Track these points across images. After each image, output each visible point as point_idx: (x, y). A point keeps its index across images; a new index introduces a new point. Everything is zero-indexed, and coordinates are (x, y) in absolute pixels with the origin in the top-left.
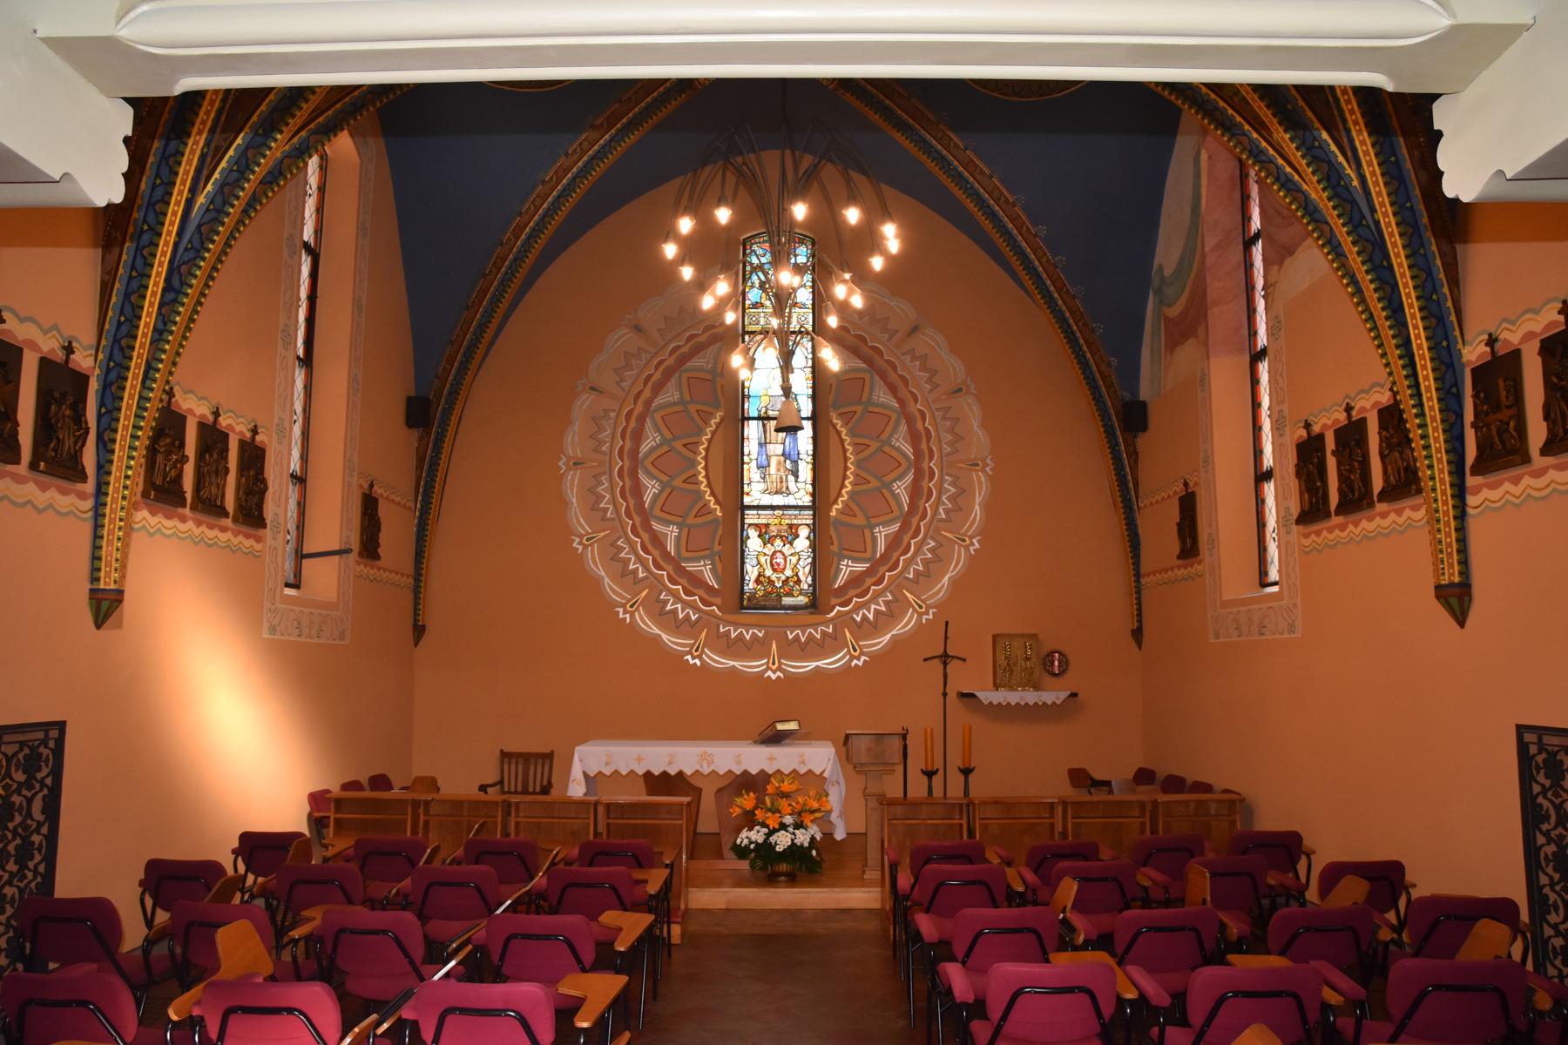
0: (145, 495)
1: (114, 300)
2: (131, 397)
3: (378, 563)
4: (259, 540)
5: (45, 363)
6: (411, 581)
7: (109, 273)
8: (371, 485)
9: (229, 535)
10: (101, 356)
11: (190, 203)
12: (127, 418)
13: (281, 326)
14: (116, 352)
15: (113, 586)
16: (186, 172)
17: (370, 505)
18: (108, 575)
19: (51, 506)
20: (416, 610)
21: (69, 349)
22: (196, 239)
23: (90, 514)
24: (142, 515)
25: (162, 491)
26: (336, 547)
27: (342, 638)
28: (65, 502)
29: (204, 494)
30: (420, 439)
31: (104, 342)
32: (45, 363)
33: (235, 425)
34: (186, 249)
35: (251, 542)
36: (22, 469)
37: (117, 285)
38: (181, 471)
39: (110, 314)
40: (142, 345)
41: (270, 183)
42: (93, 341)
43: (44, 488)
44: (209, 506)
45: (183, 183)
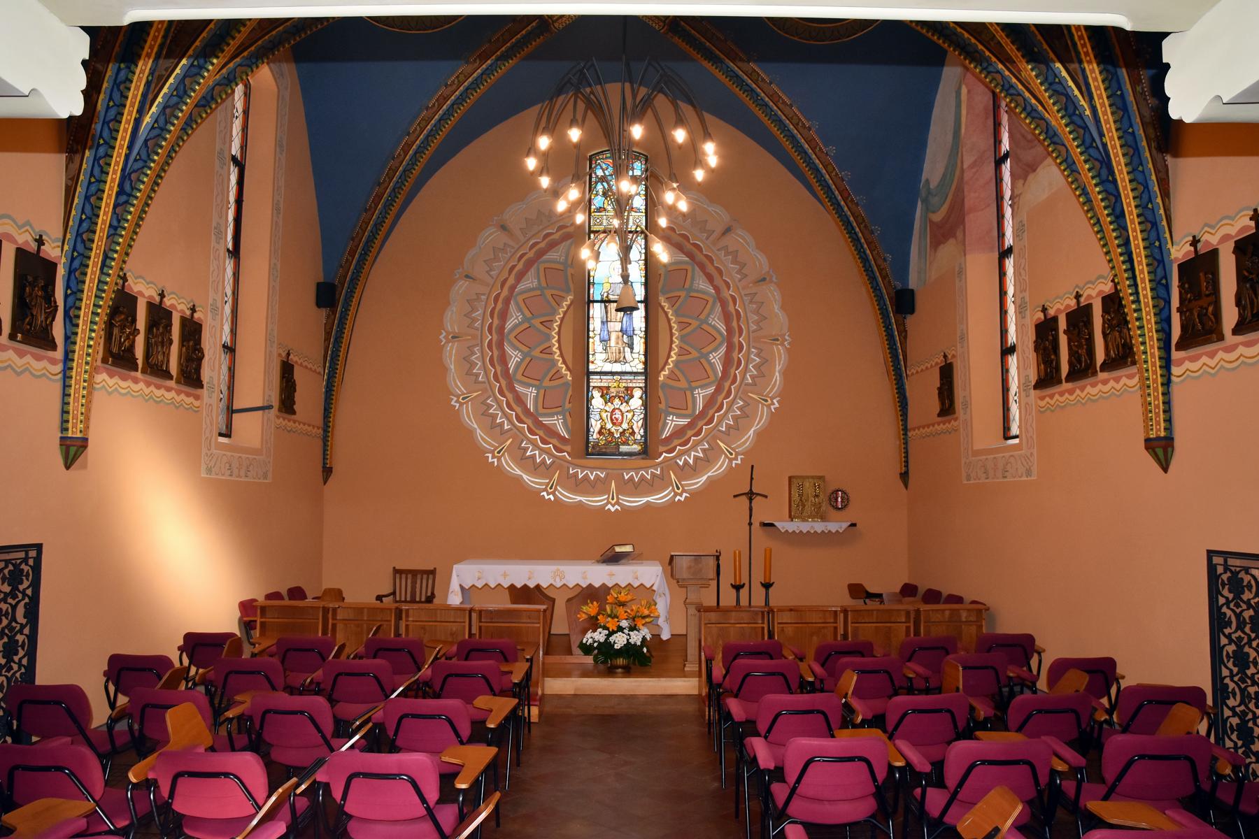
0: (104, 361)
1: (76, 201)
4: (197, 398)
6: (321, 431)
7: (72, 179)
9: (173, 394)
10: (66, 247)
11: (138, 122)
17: (287, 370)
18: (75, 426)
20: (325, 454)
21: (40, 242)
25: (120, 358)
26: (260, 404)
30: (328, 317)
31: (68, 236)
33: (178, 305)
34: (136, 160)
37: (79, 189)
38: (134, 341)
39: (73, 212)
42: (61, 236)
44: (157, 370)
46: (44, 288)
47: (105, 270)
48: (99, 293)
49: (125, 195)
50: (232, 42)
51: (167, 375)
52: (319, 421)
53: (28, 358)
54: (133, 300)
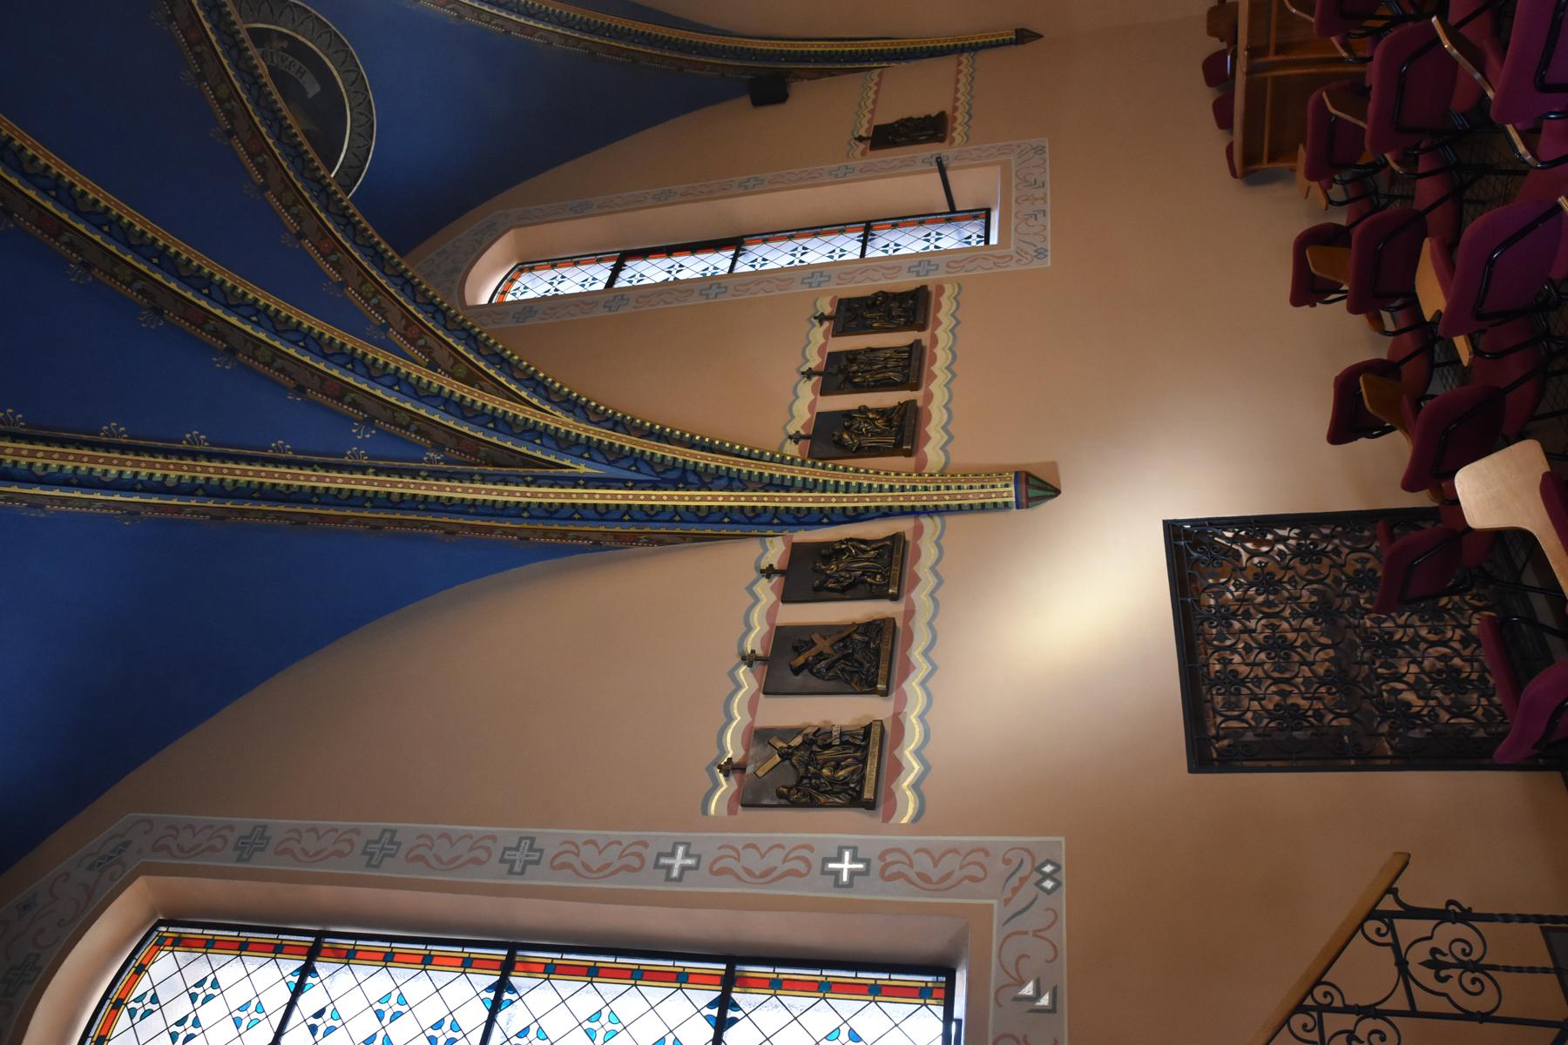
0: (908, 454)
2: (805, 500)
3: (949, 112)
4: (940, 290)
5: (825, 391)
6: (964, 58)
8: (860, 139)
9: (940, 332)
11: (589, 482)
12: (828, 500)
13: (703, 301)
14: (761, 520)
15: (1012, 488)
16: (557, 495)
17: (886, 137)
18: (1000, 495)
19: (948, 368)
20: (998, 45)
21: (769, 572)
22: (625, 463)
23: (937, 519)
24: (933, 453)
25: (901, 432)
26: (937, 176)
27: (1039, 150)
28: (928, 551)
29: (895, 377)
30: (799, 78)
32: (787, 597)
33: (818, 343)
34: (638, 471)
35: (944, 299)
36: (924, 337)
38: (876, 411)
40: (749, 499)
41: (546, 388)
42: (757, 541)
43: (916, 580)
44: (909, 368)
45: (569, 495)
46: (827, 559)
47: (787, 483)
48: (820, 487)
49: (684, 477)
50: (447, 389)
51: (916, 350)
52: (946, 65)
53: (941, 315)
54: (823, 419)
